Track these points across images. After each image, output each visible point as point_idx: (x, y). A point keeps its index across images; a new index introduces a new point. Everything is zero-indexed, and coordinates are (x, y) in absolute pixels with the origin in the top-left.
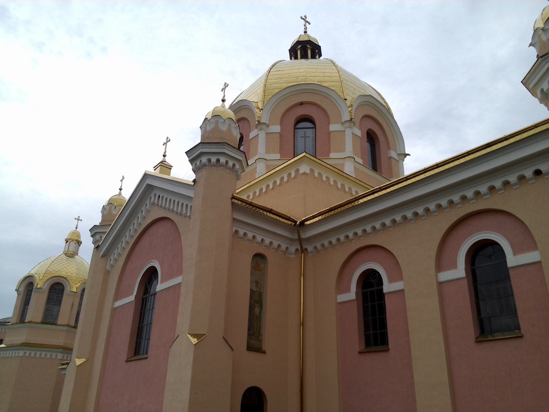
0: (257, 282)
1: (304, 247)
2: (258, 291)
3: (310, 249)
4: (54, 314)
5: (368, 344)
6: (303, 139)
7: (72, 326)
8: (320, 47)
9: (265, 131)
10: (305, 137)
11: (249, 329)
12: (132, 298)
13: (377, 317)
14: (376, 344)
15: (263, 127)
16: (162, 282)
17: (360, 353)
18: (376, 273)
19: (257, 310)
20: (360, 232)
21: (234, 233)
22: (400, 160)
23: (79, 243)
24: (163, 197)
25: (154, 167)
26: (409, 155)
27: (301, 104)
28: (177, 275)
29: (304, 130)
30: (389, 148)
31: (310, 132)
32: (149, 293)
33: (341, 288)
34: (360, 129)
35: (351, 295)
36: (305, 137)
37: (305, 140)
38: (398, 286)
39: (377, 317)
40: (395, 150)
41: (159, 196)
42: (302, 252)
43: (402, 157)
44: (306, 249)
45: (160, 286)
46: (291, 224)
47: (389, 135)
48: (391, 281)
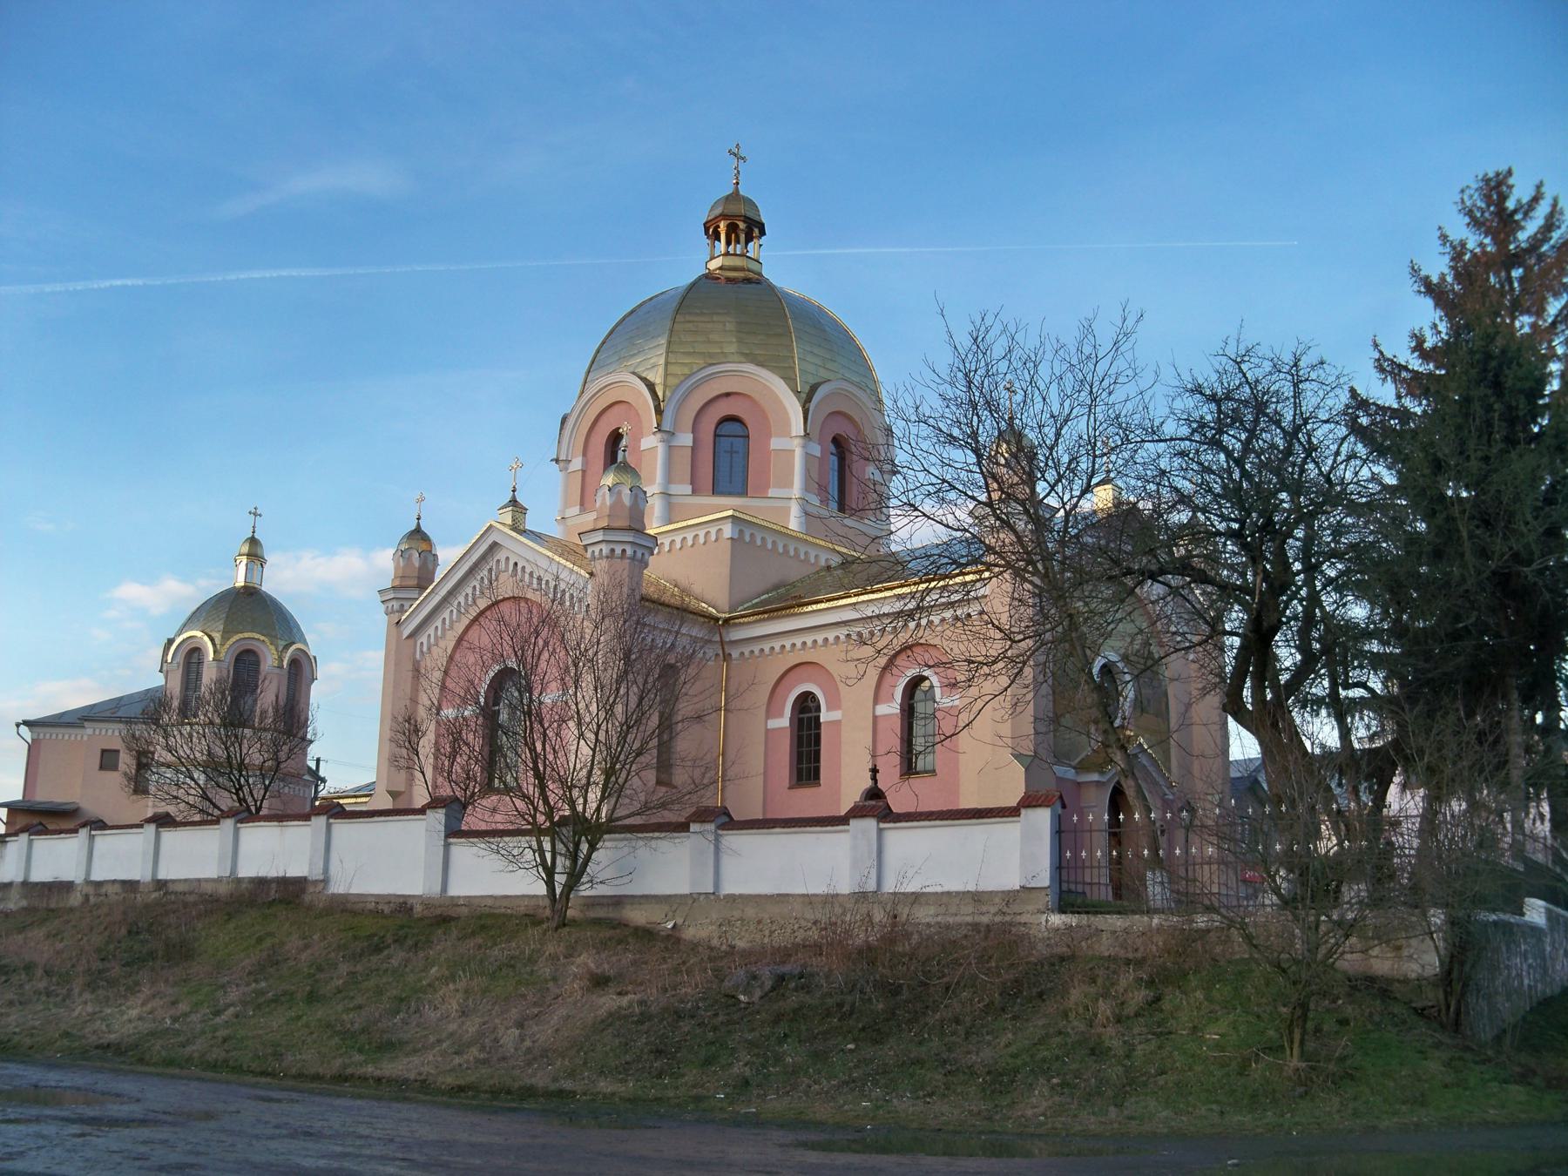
1: (727, 651)
3: (735, 654)
5: (800, 778)
6: (734, 449)
8: (763, 225)
10: (732, 452)
14: (809, 778)
17: (789, 788)
29: (731, 439)
31: (738, 442)
33: (772, 710)
35: (783, 721)
36: (732, 452)
37: (1095, 831)
38: (836, 715)
42: (724, 660)
44: (730, 655)
48: (829, 709)
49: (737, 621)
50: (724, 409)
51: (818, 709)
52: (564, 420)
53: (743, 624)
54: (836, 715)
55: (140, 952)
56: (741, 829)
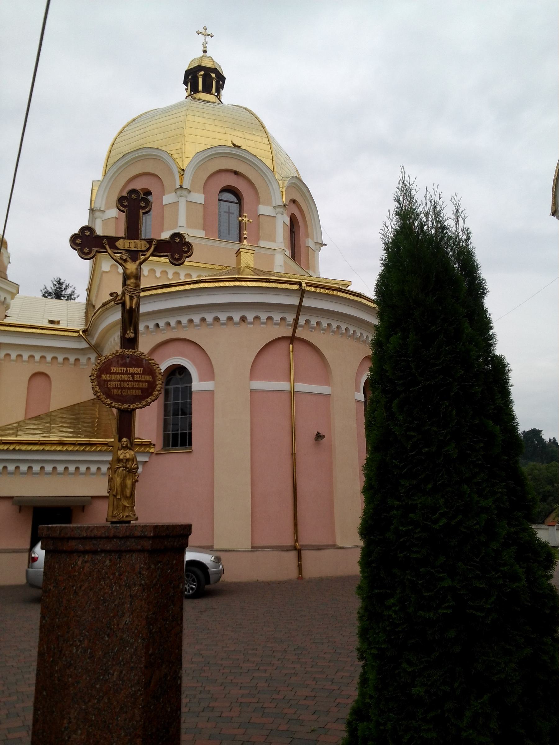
6: (227, 214)
15: (185, 193)
20: (173, 323)
25: (236, 253)
26: (326, 245)
27: (236, 173)
30: (307, 236)
36: (229, 213)
38: (208, 385)
40: (313, 239)
43: (318, 246)
47: (307, 217)
48: (201, 380)
49: (71, 435)
50: (231, 181)
51: (190, 380)
52: (223, 573)
53: (9, 284)
54: (208, 385)
55: (128, 334)
56: (167, 368)
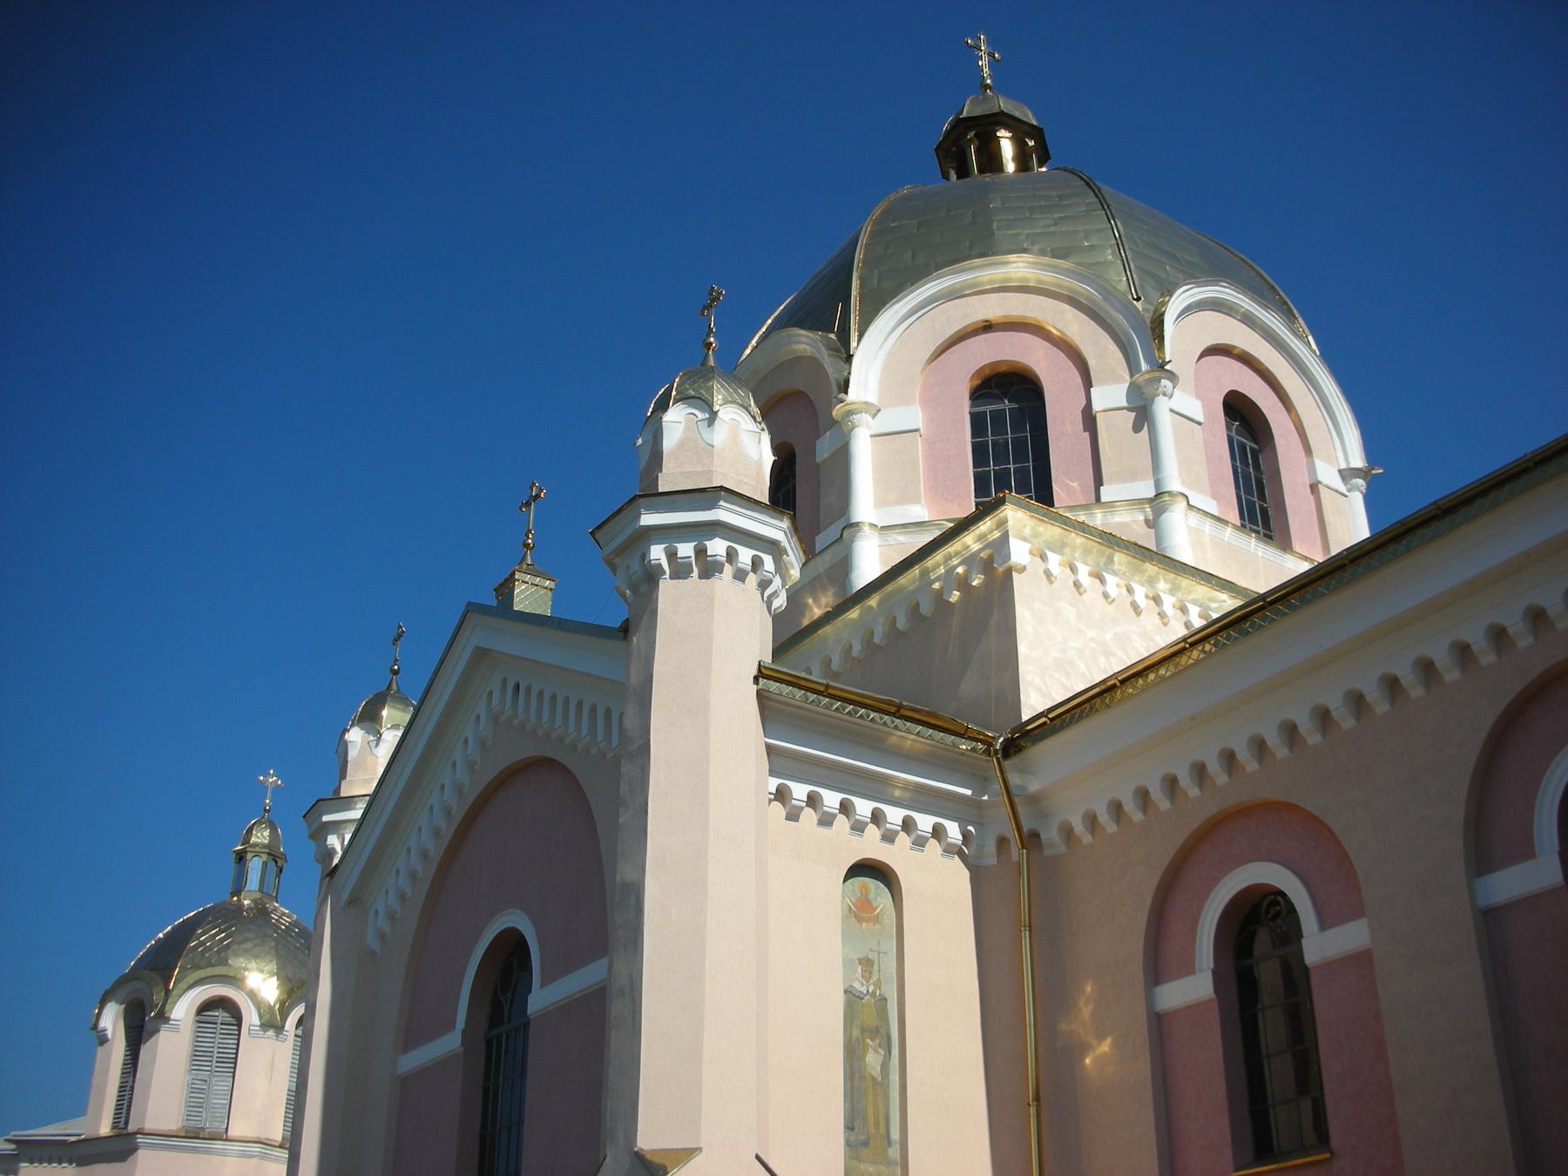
0: (867, 963)
2: (874, 993)
4: (214, 1103)
7: (276, 1141)
9: (869, 428)
11: (849, 1127)
12: (450, 1042)
13: (1012, 467)
16: (544, 984)
18: (1280, 899)
19: (873, 1060)
21: (773, 797)
22: (1349, 491)
23: (276, 863)
24: (529, 689)
27: (987, 327)
28: (592, 958)
32: (506, 1020)
34: (1198, 396)
38: (1351, 937)
39: (1012, 467)
41: (517, 687)
45: (540, 999)
46: (973, 750)
48: (1324, 924)
